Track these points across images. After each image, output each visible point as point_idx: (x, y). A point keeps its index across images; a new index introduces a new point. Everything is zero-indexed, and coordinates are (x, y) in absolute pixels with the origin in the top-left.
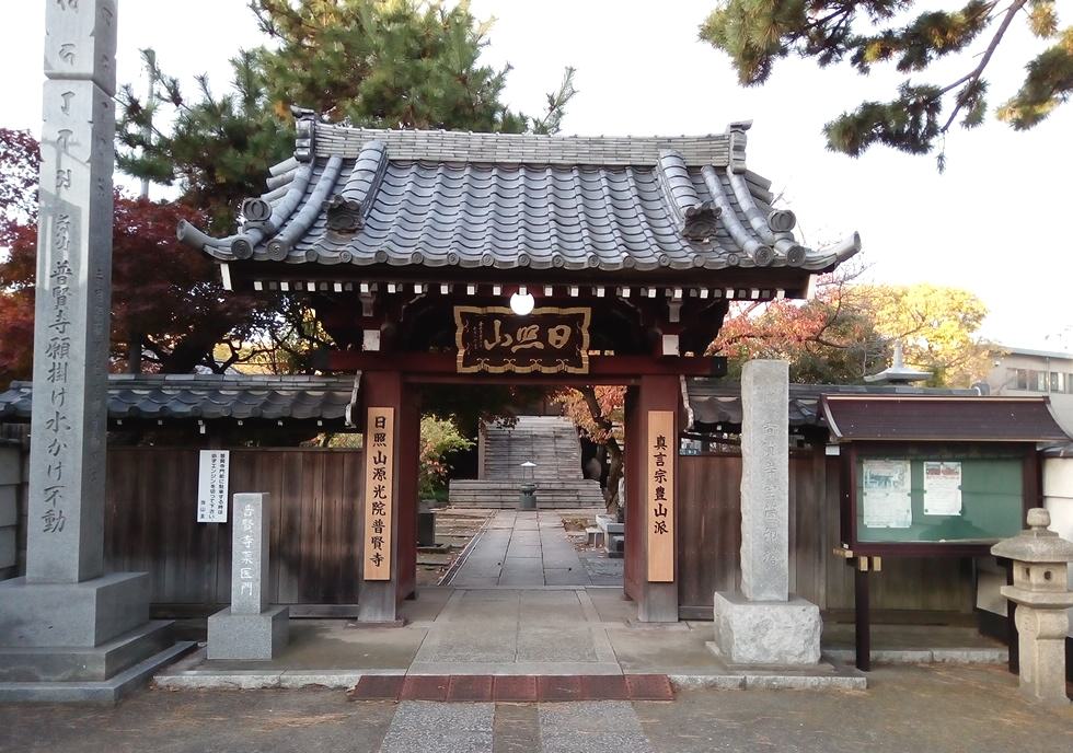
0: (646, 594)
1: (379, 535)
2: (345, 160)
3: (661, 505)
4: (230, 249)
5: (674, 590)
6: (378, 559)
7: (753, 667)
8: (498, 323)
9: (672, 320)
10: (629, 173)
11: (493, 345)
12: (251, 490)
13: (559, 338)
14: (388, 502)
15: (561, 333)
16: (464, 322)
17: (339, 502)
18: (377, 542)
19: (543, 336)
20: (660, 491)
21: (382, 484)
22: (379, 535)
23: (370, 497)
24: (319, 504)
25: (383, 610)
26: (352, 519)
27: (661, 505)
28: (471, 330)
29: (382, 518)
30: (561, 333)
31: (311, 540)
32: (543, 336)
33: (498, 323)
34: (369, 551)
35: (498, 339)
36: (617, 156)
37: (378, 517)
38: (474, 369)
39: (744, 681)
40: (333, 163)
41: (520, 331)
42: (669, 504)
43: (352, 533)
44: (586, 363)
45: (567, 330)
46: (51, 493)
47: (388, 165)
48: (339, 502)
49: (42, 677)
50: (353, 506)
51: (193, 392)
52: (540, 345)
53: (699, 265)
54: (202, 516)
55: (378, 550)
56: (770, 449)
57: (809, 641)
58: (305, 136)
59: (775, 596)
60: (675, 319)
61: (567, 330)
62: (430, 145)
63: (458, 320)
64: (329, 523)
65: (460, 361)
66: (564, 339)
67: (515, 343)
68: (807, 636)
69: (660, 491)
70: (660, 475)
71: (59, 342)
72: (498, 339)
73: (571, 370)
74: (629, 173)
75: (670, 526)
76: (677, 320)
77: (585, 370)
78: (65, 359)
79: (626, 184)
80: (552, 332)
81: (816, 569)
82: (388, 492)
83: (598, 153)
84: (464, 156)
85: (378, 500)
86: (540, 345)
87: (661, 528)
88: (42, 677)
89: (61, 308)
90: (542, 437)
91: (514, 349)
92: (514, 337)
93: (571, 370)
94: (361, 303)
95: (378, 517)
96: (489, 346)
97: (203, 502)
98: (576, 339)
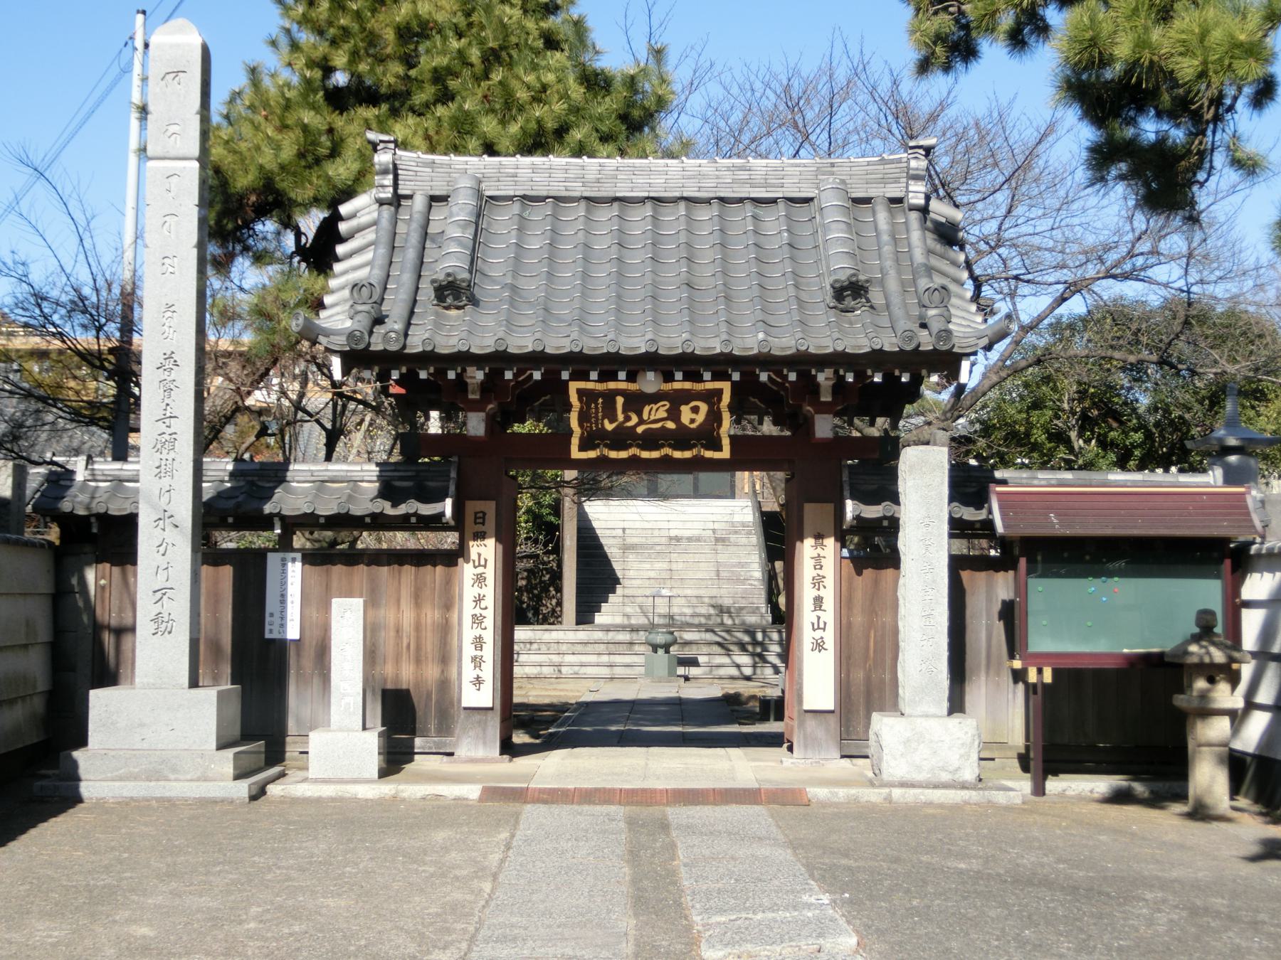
0: (802, 724)
1: (479, 653)
2: (434, 199)
3: (819, 618)
4: (344, 338)
5: (833, 721)
6: (478, 681)
7: (904, 785)
8: (620, 400)
9: (823, 399)
10: (781, 205)
11: (614, 425)
12: (350, 594)
13: (693, 416)
14: (489, 614)
15: (695, 410)
16: (580, 399)
17: (431, 615)
18: (477, 661)
19: (674, 414)
20: (818, 601)
21: (482, 592)
22: (479, 653)
23: (468, 609)
24: (407, 616)
25: (485, 743)
26: (445, 631)
27: (819, 618)
28: (589, 407)
29: (484, 633)
30: (695, 410)
31: (397, 660)
32: (674, 414)
33: (620, 400)
34: (469, 672)
35: (621, 417)
36: (766, 185)
37: (478, 632)
38: (592, 454)
39: (890, 795)
40: (419, 203)
41: (647, 409)
42: (829, 615)
43: (445, 656)
44: (726, 443)
45: (704, 408)
46: (159, 595)
47: (485, 203)
48: (431, 615)
49: (172, 777)
50: (447, 620)
51: (260, 484)
52: (671, 425)
53: (840, 349)
54: (271, 631)
55: (478, 671)
56: (927, 547)
57: (965, 756)
58: (385, 172)
59: (933, 710)
60: (826, 397)
61: (704, 408)
62: (537, 178)
63: (574, 398)
64: (418, 638)
65: (575, 442)
66: (700, 418)
67: (641, 422)
68: (962, 751)
69: (818, 601)
70: (818, 582)
71: (167, 437)
72: (621, 417)
73: (709, 454)
74: (781, 205)
75: (830, 642)
76: (829, 399)
77: (725, 454)
78: (172, 454)
79: (773, 221)
80: (686, 411)
81: (1010, 696)
82: (489, 602)
83: (743, 182)
84: (578, 190)
85: (478, 611)
86: (671, 425)
87: (819, 646)
88: (172, 777)
89: (167, 401)
90: (689, 539)
91: (640, 430)
92: (640, 414)
93: (709, 454)
94: (466, 384)
95: (478, 632)
96: (609, 427)
97: (272, 615)
98: (714, 417)
